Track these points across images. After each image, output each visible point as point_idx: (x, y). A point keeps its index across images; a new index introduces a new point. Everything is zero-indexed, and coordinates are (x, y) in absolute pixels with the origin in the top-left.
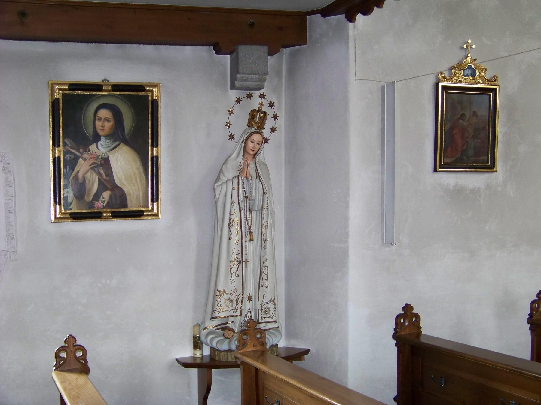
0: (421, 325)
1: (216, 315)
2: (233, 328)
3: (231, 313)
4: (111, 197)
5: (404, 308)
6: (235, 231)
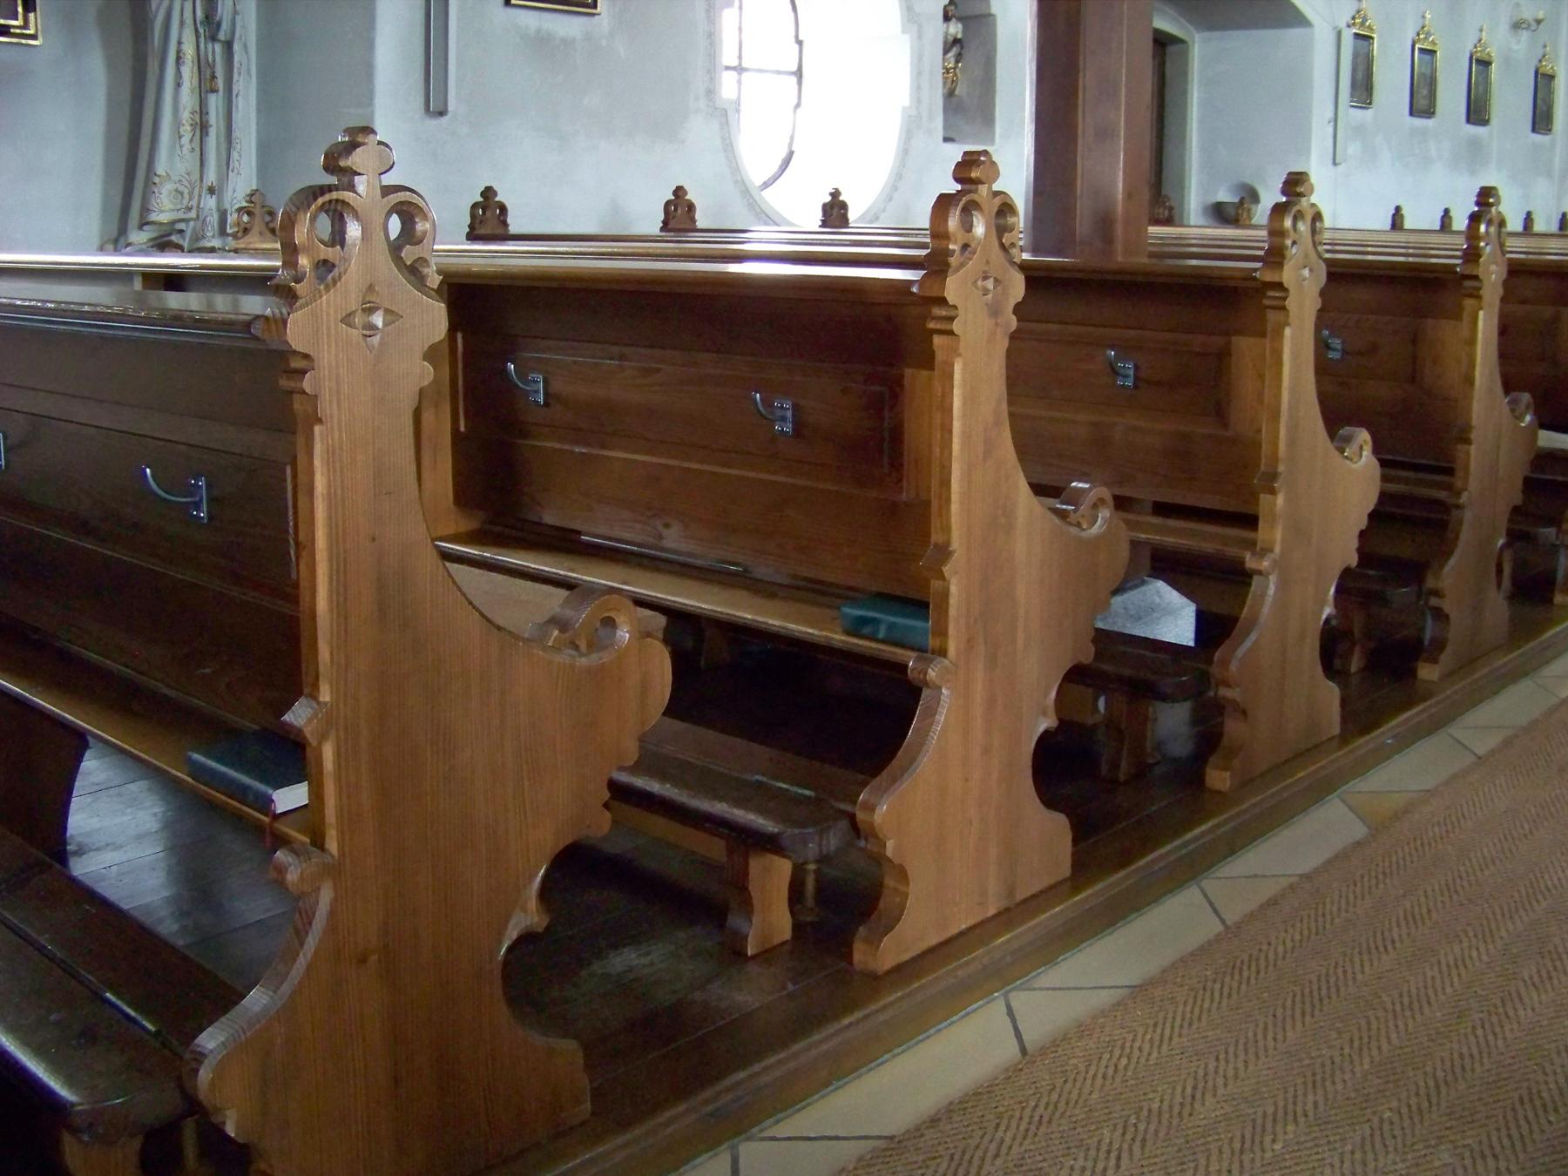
0: (509, 220)
1: (154, 217)
2: (181, 242)
3: (181, 215)
4: (288, 706)
5: (482, 194)
6: (188, 71)
